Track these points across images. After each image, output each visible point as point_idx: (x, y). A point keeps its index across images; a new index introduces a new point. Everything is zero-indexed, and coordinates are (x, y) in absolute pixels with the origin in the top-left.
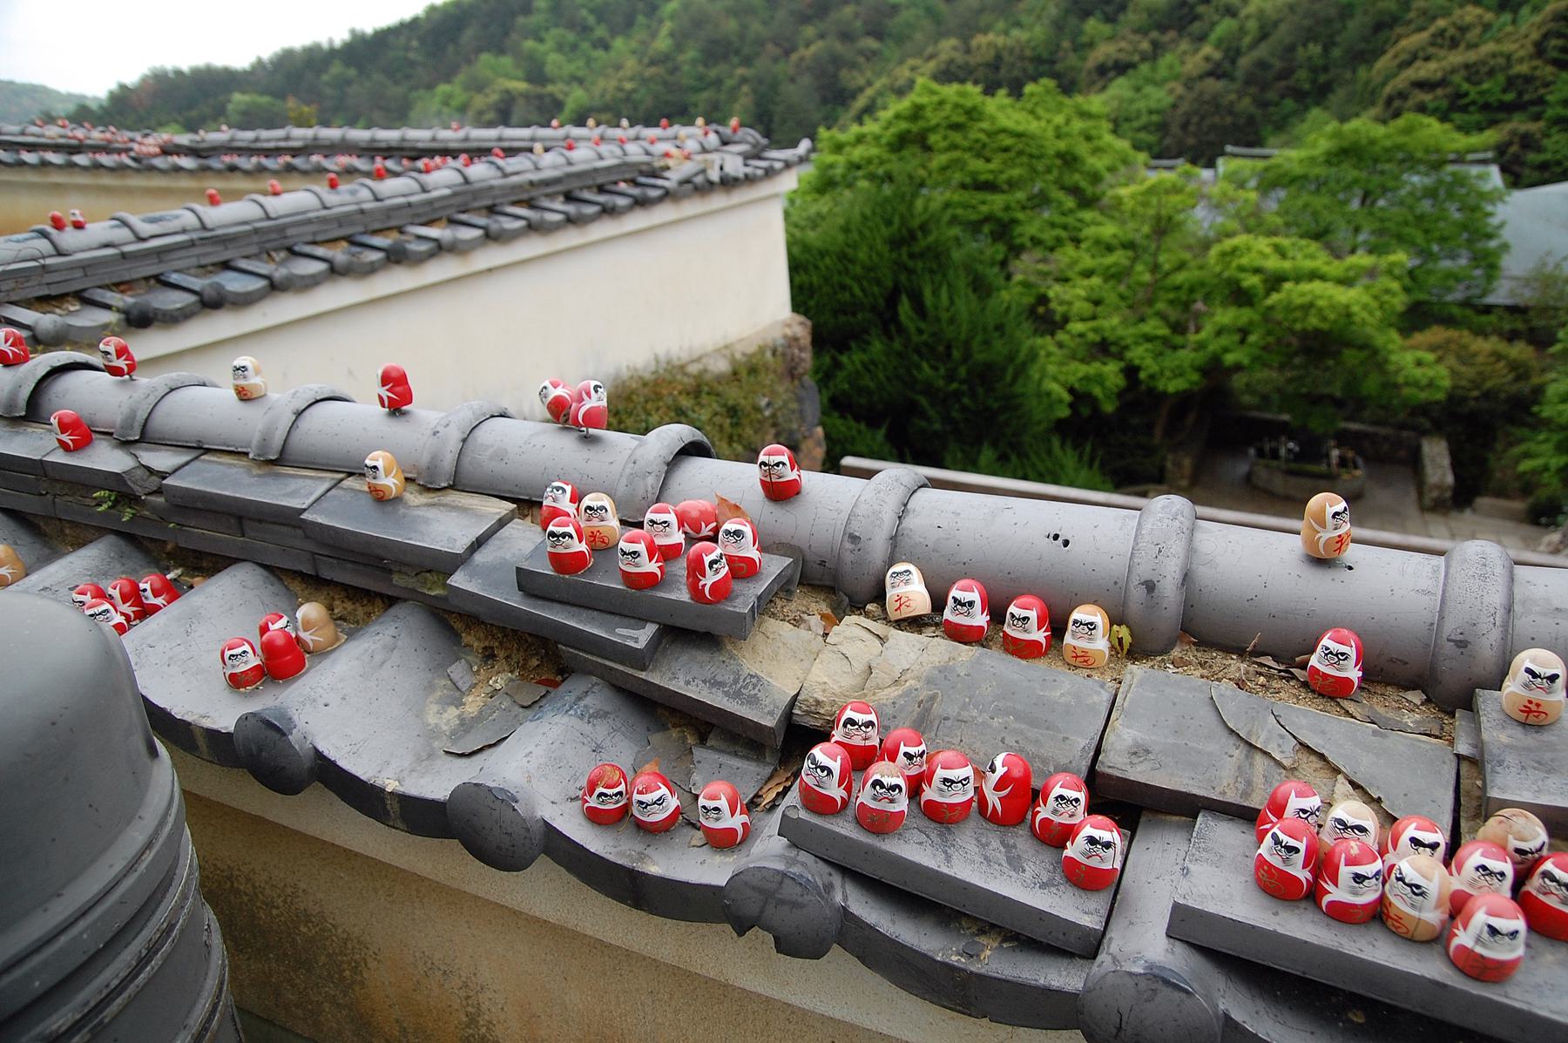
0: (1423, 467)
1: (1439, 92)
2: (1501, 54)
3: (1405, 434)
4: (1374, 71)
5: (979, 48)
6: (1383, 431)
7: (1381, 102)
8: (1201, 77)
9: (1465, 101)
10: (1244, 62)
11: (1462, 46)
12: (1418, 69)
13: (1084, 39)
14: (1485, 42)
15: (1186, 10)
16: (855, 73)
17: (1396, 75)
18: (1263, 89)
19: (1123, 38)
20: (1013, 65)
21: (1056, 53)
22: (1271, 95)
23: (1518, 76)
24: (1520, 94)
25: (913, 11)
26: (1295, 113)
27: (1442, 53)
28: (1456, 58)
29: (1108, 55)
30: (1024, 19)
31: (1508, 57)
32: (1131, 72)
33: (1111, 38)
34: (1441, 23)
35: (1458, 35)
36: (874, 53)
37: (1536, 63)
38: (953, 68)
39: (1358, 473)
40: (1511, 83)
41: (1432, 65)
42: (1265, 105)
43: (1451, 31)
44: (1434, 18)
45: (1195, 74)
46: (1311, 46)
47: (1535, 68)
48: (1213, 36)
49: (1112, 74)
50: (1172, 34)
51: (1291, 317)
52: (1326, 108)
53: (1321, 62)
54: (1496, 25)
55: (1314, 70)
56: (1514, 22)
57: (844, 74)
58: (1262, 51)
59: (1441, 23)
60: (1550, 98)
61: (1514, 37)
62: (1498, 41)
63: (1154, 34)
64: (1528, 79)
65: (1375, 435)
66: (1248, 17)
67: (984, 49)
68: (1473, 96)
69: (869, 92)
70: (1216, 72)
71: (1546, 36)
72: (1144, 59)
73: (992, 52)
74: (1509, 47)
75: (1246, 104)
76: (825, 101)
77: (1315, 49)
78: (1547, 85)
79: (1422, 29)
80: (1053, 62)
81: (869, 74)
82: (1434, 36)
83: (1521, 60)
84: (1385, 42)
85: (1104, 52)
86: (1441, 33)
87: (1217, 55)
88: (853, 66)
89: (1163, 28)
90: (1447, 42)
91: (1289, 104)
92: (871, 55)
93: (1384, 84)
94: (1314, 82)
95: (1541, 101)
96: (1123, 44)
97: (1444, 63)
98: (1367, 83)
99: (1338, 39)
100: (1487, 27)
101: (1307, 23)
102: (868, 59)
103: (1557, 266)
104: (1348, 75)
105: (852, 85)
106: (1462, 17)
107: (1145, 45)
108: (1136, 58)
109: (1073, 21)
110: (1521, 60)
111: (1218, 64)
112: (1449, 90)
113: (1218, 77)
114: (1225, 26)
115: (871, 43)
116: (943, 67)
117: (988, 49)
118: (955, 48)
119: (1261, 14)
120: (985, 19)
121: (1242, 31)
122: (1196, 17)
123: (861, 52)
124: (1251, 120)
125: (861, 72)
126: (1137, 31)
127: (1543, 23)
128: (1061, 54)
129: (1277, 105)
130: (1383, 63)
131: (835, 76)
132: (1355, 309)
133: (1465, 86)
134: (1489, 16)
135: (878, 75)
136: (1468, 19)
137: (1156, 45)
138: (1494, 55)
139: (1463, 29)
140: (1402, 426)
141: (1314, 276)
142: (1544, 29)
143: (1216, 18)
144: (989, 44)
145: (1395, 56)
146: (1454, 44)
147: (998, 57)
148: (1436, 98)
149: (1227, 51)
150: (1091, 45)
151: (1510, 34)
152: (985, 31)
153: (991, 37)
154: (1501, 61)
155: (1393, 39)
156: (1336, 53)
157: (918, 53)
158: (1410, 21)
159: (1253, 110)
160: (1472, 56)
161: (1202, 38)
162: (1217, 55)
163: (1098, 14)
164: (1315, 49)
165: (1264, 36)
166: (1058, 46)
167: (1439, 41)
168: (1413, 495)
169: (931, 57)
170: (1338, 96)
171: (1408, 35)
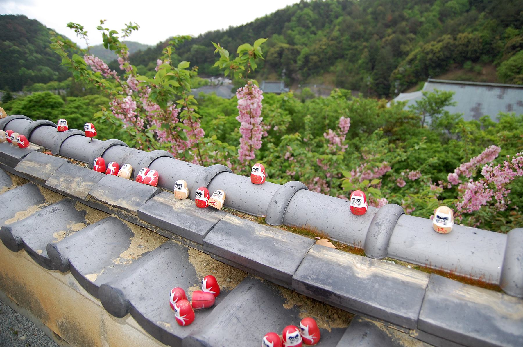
5: (460, 38)
13: (506, 35)
16: (406, 46)
25: (428, 24)
36: (413, 39)
38: (449, 45)
49: (518, 49)
57: (402, 46)
69: (413, 53)
73: (466, 40)
76: (394, 56)
88: (405, 43)
92: (412, 40)
102: (411, 41)
109: (501, 28)
115: (412, 35)
116: (445, 45)
118: (449, 38)
120: (461, 28)
123: (408, 39)
128: (495, 41)
131: (399, 47)
147: (469, 42)
152: (463, 32)
153: (465, 34)
163: (512, 25)
166: (494, 38)
169: (439, 42)
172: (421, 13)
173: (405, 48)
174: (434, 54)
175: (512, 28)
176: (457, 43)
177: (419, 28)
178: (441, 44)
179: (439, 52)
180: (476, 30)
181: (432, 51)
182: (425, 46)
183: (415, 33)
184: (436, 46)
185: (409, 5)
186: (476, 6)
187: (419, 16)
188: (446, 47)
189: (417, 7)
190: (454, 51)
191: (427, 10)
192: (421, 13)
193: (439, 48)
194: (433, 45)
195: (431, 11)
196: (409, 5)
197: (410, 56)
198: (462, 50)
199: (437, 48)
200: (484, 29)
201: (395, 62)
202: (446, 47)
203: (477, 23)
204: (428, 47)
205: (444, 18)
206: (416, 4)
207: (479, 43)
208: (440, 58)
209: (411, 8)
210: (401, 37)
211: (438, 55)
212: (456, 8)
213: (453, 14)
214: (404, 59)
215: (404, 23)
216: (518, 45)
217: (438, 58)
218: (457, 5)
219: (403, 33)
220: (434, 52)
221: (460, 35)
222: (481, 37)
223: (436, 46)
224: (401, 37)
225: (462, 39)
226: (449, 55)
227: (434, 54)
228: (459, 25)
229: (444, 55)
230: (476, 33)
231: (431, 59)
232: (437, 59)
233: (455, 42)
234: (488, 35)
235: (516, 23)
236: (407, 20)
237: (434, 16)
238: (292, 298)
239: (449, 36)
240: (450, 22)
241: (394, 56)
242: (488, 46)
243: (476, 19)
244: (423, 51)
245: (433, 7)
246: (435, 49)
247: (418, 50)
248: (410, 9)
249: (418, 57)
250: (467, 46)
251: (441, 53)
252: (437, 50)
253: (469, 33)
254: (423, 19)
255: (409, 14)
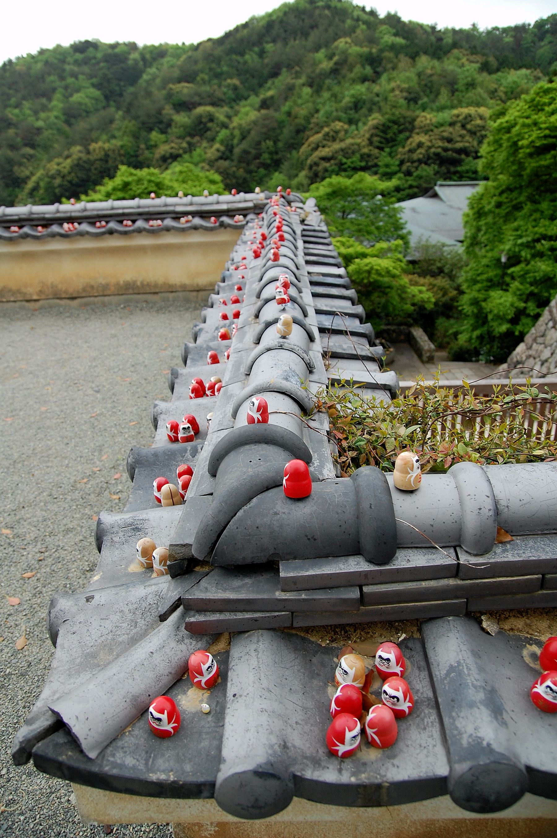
0: (416, 342)
1: (332, 162)
2: (356, 144)
3: (402, 328)
4: (300, 153)
5: (94, 150)
6: (393, 328)
7: (307, 168)
8: (217, 160)
9: (346, 166)
10: (237, 151)
11: (338, 141)
12: (321, 151)
13: (152, 143)
14: (347, 138)
15: (202, 126)
16: (23, 168)
17: (311, 155)
18: (248, 164)
19: (172, 142)
20: (115, 159)
21: (137, 151)
22: (253, 167)
23: (364, 154)
24: (367, 162)
25: (50, 131)
26: (266, 175)
27: (330, 144)
28: (337, 146)
29: (166, 151)
30: (117, 134)
31: (359, 145)
32: (179, 159)
33: (165, 142)
34: (326, 129)
35: (334, 135)
36: (32, 156)
37: (371, 148)
38: (81, 162)
39: (392, 350)
40: (362, 157)
41: (327, 150)
42: (250, 172)
43: (332, 133)
44: (322, 127)
45: (213, 158)
46: (268, 141)
47: (370, 150)
48: (218, 139)
49: (170, 161)
50: (197, 139)
51: (361, 277)
52: (280, 173)
53: (273, 149)
54: (350, 131)
55: (271, 153)
56: (357, 129)
57: (16, 169)
58: (244, 145)
59: (326, 129)
60: (380, 164)
61: (359, 136)
62: (353, 138)
63: (188, 139)
64: (369, 156)
65: (389, 330)
66: (234, 128)
67: (97, 151)
68: (349, 164)
69: (34, 179)
70: (223, 157)
71: (372, 136)
72: (185, 152)
73: (103, 153)
74: (358, 141)
75: (241, 172)
76: (7, 186)
77: (270, 143)
78: (377, 158)
79: (317, 133)
80: (137, 156)
81: (31, 168)
82: (324, 135)
83: (364, 147)
84: (303, 139)
85: (164, 149)
86: (327, 134)
87: (222, 148)
88: (20, 164)
89: (192, 136)
90: (331, 139)
91: (262, 171)
92: (30, 158)
93: (306, 159)
94: (272, 159)
95: (376, 165)
96: (173, 145)
97: (331, 149)
98: (298, 159)
99: (280, 138)
100: (346, 131)
101: (264, 130)
102: (28, 160)
103: (427, 240)
104: (289, 156)
105: (22, 175)
106: (335, 127)
107: (185, 145)
108: (181, 152)
109: (144, 134)
110: (364, 147)
111: (223, 153)
112: (337, 161)
113: (226, 159)
114: (223, 134)
115: (28, 150)
116: (75, 162)
117: (100, 151)
118: (80, 152)
119: (240, 127)
120: (94, 135)
121: (233, 136)
122: (208, 129)
123: (24, 156)
124: (245, 180)
125: (27, 168)
126: (179, 138)
127: (369, 130)
128: (140, 152)
129: (256, 172)
130: (304, 149)
131: (11, 171)
132: (391, 268)
133: (344, 160)
134: (346, 127)
135: (37, 168)
136: (338, 128)
137: (189, 144)
138: (353, 144)
139: (337, 132)
140: (401, 324)
141: (364, 256)
142: (370, 133)
143: (218, 129)
144: (100, 148)
145: (309, 146)
146: (334, 139)
147: (107, 155)
148: (331, 166)
149: (227, 146)
150: (156, 146)
151: (356, 135)
152: (96, 141)
153: (100, 144)
154: (356, 147)
155: (306, 138)
156: (280, 145)
157: (60, 155)
158: (312, 129)
159: (244, 175)
160: (343, 145)
161: (212, 140)
162: (222, 148)
163: (156, 129)
164: (270, 143)
165: (243, 138)
166: (138, 147)
167: (327, 138)
168: (415, 357)
169: (68, 157)
170: (285, 166)
171: (312, 136)
172: (36, 113)
173: (21, 172)
174: (63, 177)
175: (157, 132)
176: (92, 158)
177: (37, 138)
178: (69, 161)
179: (70, 173)
180: (114, 137)
181: (59, 172)
182: (48, 166)
183: (33, 146)
184: (63, 165)
185: (13, 100)
186: (115, 101)
187: (31, 119)
188: (78, 166)
189: (26, 104)
190: (90, 170)
191: (44, 108)
192: (36, 113)
193: (68, 167)
194: (58, 164)
195: (50, 110)
196: (13, 100)
197: (30, 185)
198: (101, 167)
199: (65, 167)
200: (123, 135)
201: (10, 196)
202: (78, 165)
203: (114, 126)
204: (53, 167)
205: (73, 120)
206: (24, 98)
207: (120, 155)
208: (74, 182)
209: (17, 106)
210: (10, 153)
211: (69, 178)
212: (86, 104)
213: (84, 114)
214: (22, 189)
215: (11, 132)
216: (168, 155)
217: (70, 182)
218: (87, 100)
219: (13, 147)
220: (62, 174)
221: (93, 146)
222: (122, 147)
223: (63, 165)
224: (10, 153)
225: (97, 151)
226: (85, 177)
227: (63, 177)
228: (91, 130)
229: (78, 177)
230: (114, 141)
231: (60, 186)
232: (69, 185)
233: (88, 156)
234: (130, 144)
235: (161, 126)
236: (15, 126)
237: (56, 117)
238: (460, 734)
239: (78, 148)
240: (82, 125)
241: (7, 186)
242: (134, 159)
243: (112, 121)
244: (47, 174)
245: (54, 103)
246: (62, 170)
247: (40, 173)
248: (16, 107)
249: (42, 184)
250: (107, 161)
251: (73, 174)
252: (66, 171)
253: (104, 143)
254: (40, 124)
255: (17, 116)
